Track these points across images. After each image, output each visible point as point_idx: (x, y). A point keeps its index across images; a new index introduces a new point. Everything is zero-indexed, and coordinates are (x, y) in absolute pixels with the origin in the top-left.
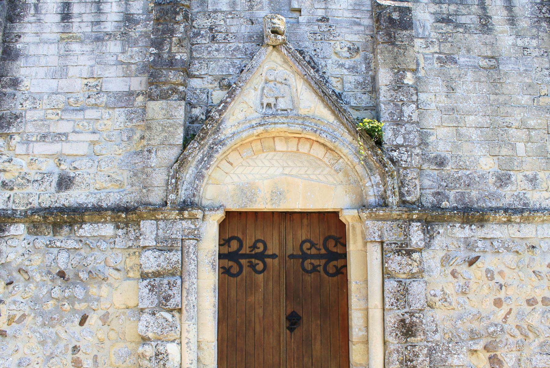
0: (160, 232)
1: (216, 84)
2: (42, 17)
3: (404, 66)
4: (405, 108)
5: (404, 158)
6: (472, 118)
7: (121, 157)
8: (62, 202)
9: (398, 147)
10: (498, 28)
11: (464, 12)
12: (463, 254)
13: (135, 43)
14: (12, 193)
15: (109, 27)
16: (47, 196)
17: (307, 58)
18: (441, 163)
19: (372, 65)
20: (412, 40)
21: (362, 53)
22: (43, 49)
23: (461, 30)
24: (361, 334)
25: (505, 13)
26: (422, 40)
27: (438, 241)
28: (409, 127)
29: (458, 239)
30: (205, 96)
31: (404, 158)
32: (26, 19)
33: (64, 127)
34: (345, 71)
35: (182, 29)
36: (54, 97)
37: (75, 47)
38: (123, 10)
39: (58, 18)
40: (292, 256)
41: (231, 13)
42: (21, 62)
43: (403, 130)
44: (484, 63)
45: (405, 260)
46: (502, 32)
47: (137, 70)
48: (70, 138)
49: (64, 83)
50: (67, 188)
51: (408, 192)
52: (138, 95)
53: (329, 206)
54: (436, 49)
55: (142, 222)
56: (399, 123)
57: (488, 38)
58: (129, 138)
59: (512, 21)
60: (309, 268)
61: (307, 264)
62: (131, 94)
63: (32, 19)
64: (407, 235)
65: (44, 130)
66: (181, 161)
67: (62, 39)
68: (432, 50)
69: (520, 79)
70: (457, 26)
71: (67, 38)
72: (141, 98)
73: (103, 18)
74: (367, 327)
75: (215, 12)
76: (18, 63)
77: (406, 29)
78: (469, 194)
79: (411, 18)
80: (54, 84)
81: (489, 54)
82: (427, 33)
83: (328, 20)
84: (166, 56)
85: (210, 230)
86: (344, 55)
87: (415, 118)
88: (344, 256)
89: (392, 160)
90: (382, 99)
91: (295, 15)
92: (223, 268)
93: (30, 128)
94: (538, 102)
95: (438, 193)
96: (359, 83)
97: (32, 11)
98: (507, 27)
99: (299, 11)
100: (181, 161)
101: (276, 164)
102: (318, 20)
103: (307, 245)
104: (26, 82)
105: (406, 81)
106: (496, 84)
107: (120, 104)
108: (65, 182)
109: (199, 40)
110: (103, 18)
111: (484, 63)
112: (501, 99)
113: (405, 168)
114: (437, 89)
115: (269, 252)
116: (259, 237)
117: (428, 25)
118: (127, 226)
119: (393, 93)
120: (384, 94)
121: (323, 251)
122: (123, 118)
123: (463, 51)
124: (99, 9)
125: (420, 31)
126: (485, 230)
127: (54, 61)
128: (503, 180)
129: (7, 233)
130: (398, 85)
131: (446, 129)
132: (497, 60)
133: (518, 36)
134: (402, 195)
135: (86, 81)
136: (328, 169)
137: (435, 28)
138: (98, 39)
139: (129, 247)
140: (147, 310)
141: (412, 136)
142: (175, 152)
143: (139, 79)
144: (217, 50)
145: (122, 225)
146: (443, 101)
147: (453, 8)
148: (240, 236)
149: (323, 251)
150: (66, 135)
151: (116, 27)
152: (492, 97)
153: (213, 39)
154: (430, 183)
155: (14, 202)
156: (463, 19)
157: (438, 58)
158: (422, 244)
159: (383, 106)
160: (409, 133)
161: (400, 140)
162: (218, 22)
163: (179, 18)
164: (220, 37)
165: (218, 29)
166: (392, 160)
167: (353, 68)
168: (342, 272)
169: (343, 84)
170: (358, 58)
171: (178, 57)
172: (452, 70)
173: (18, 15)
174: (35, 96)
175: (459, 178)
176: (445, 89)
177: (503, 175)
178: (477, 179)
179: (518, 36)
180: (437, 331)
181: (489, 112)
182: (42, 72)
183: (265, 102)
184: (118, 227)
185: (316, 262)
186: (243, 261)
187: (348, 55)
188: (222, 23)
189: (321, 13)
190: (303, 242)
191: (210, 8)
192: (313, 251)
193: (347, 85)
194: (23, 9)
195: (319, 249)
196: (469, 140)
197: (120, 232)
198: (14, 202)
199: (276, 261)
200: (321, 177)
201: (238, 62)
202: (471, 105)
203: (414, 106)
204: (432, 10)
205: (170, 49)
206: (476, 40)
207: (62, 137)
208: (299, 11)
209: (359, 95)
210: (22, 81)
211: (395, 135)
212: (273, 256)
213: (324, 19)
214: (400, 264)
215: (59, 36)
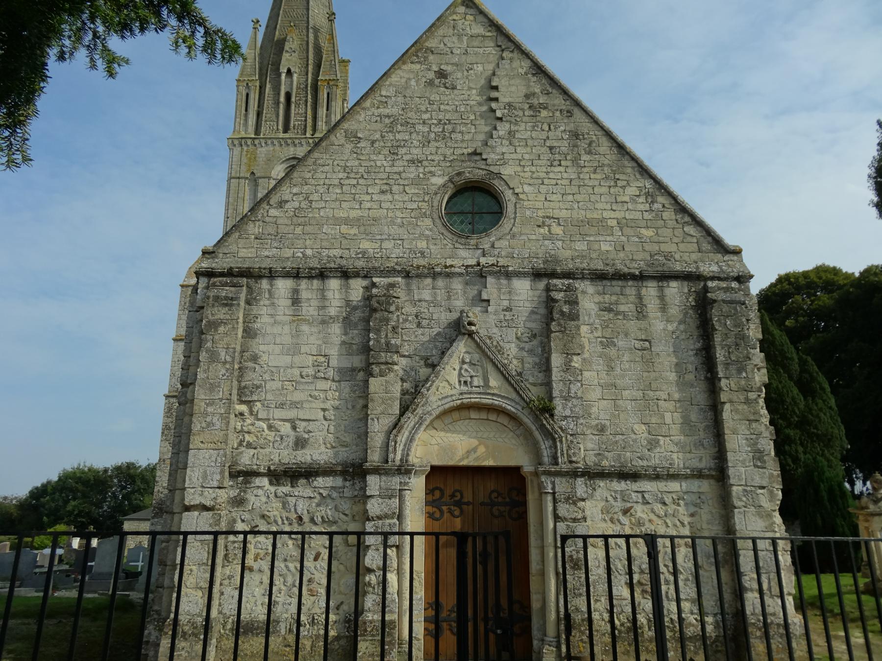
0: (383, 483)
1: (422, 362)
2: (276, 301)
3: (572, 352)
4: (572, 386)
5: (571, 427)
6: (627, 392)
7: (347, 422)
8: (299, 459)
9: (566, 417)
10: (651, 315)
11: (623, 301)
12: (619, 505)
13: (355, 326)
14: (255, 451)
15: (333, 311)
16: (283, 455)
17: (495, 343)
18: (602, 429)
19: (547, 348)
20: (579, 329)
21: (539, 338)
22: (277, 330)
23: (620, 317)
24: (538, 567)
25: (658, 302)
26: (588, 327)
27: (598, 493)
28: (575, 401)
29: (616, 492)
30: (413, 373)
31: (571, 427)
32: (262, 303)
33: (298, 396)
34: (525, 353)
35: (395, 318)
36: (289, 370)
37: (305, 328)
38: (344, 297)
39: (289, 302)
40: (482, 504)
41: (433, 302)
42: (259, 340)
43: (570, 404)
44: (638, 344)
45: (572, 508)
46: (655, 319)
47: (358, 349)
48: (304, 406)
49: (297, 359)
50: (303, 447)
51: (574, 453)
52: (359, 371)
53: (512, 463)
54: (599, 334)
55: (368, 477)
56: (567, 398)
57: (643, 324)
58: (353, 407)
59: (664, 308)
60: (496, 513)
61: (495, 511)
62: (353, 370)
63: (267, 302)
64: (574, 488)
65: (282, 399)
66: (396, 425)
67: (294, 321)
68: (596, 335)
69: (669, 359)
70: (618, 313)
71: (297, 319)
72: (361, 374)
73: (327, 304)
74: (543, 562)
75: (420, 301)
76: (257, 340)
77: (573, 320)
78: (625, 455)
79: (578, 311)
80: (288, 359)
81: (643, 337)
82: (592, 321)
83: (511, 310)
84: (383, 341)
85: (418, 484)
86: (525, 339)
87: (579, 395)
88: (524, 504)
89: (561, 428)
90: (554, 378)
91: (485, 304)
92: (428, 513)
93: (269, 396)
94: (684, 378)
95: (599, 454)
96: (536, 364)
97: (267, 296)
98: (659, 314)
99: (488, 301)
100: (396, 425)
101: (471, 429)
102: (503, 310)
103: (495, 495)
104: (265, 357)
105: (573, 364)
106: (649, 363)
107: (344, 379)
108: (300, 443)
109: (407, 325)
110: (327, 304)
111: (638, 344)
112: (653, 375)
113: (571, 435)
114: (600, 368)
115: (465, 500)
116: (457, 487)
117: (593, 313)
118: (354, 479)
119: (562, 374)
120: (556, 375)
121: (507, 500)
122: (347, 390)
123: (622, 336)
124: (324, 296)
125: (586, 318)
126: (638, 484)
127: (287, 340)
128: (653, 444)
129: (253, 485)
130: (567, 368)
131: (605, 402)
132: (650, 343)
133: (667, 321)
134: (569, 456)
135: (315, 358)
136: (512, 434)
137: (599, 316)
138: (323, 322)
139: (356, 496)
140: (373, 547)
141: (577, 410)
142: (392, 419)
143: (360, 357)
144: (422, 335)
145: (349, 478)
146: (604, 378)
147: (614, 298)
148: (442, 486)
149: (507, 500)
150: (301, 402)
151: (339, 312)
152: (645, 374)
153: (419, 325)
154: (592, 446)
155: (258, 459)
156: (622, 308)
157: (601, 342)
158: (585, 496)
159: (554, 385)
160: (575, 406)
161: (568, 412)
162: (422, 310)
163: (393, 308)
164: (424, 323)
165: (423, 315)
166: (561, 428)
167: (532, 350)
168: (523, 516)
169: (523, 364)
170: (535, 342)
171: (393, 342)
172: (612, 352)
173: (255, 299)
174: (272, 369)
175: (616, 442)
176: (606, 368)
177: (652, 440)
178: (631, 443)
179: (667, 321)
180: (599, 566)
181: (641, 388)
182: (277, 349)
183: (462, 379)
184: (345, 480)
185: (502, 508)
186: (444, 508)
187: (527, 340)
188: (426, 310)
189: (506, 303)
190: (493, 491)
191: (416, 298)
192: (500, 499)
193: (527, 365)
194: (259, 294)
195: (504, 498)
196: (625, 410)
197: (348, 484)
198: (258, 459)
199: (471, 507)
200: (506, 440)
201: (439, 344)
202: (627, 381)
203: (579, 385)
204: (597, 300)
205: (387, 335)
206: (633, 325)
207: (295, 405)
208: (488, 301)
209: (536, 373)
210: (261, 356)
211: (564, 408)
212: (468, 504)
213: (508, 309)
214: (568, 511)
215: (291, 318)
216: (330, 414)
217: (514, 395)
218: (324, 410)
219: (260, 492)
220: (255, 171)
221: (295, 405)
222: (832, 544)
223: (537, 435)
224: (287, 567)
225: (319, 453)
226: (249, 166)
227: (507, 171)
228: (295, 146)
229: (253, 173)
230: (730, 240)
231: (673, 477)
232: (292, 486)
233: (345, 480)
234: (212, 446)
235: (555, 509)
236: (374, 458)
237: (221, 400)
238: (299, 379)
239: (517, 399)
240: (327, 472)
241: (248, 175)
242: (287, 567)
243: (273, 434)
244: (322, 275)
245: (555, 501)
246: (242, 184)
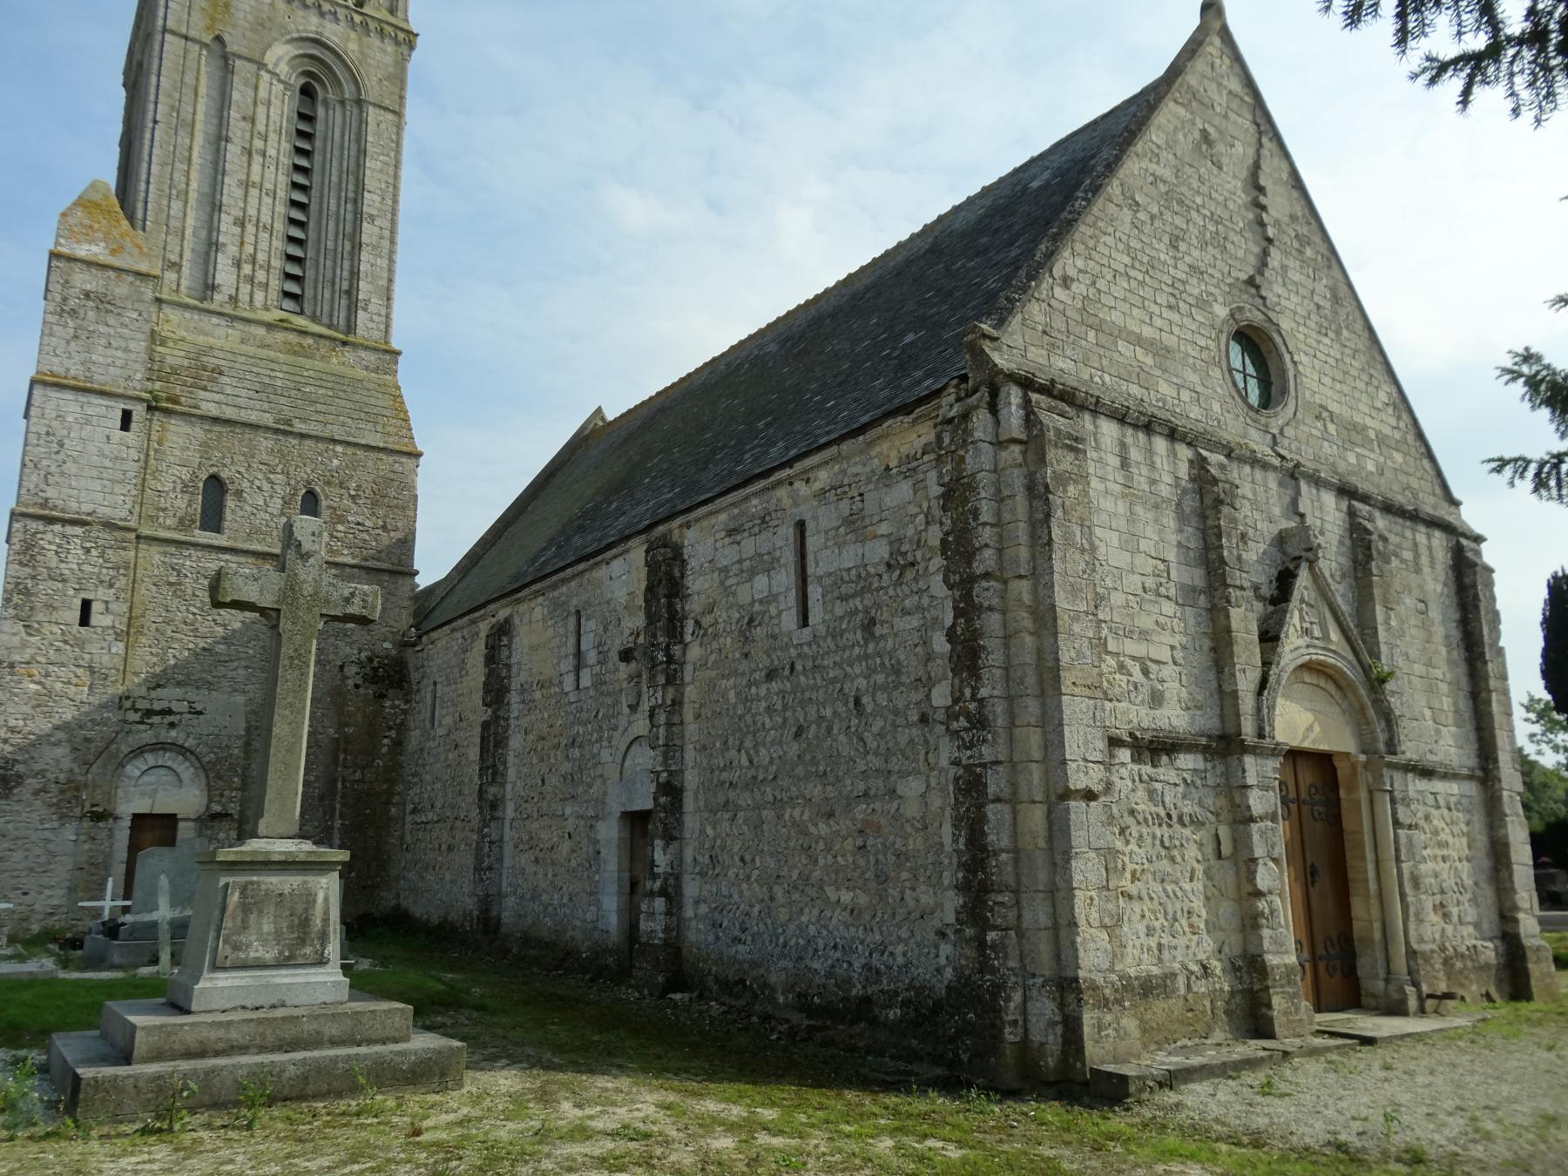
33: (1146, 622)
197: (1209, 766)
216: (1179, 655)
217: (1351, 657)
218: (1172, 648)
219: (1123, 771)
220: (226, 37)
221: (1144, 635)
222: (337, 842)
223: (1371, 712)
224: (1165, 890)
225: (1174, 717)
226: (213, 19)
227: (1286, 324)
228: (322, 15)
229: (219, 39)
230: (1457, 493)
231: (1447, 776)
232: (1154, 766)
233: (1206, 760)
234: (1088, 692)
235: (1394, 814)
236: (1248, 729)
237: (1086, 613)
238: (1140, 591)
239: (1355, 662)
240: (1190, 748)
241: (207, 38)
242: (1165, 890)
243: (1125, 678)
244: (1148, 426)
245: (1393, 801)
246: (193, 55)
